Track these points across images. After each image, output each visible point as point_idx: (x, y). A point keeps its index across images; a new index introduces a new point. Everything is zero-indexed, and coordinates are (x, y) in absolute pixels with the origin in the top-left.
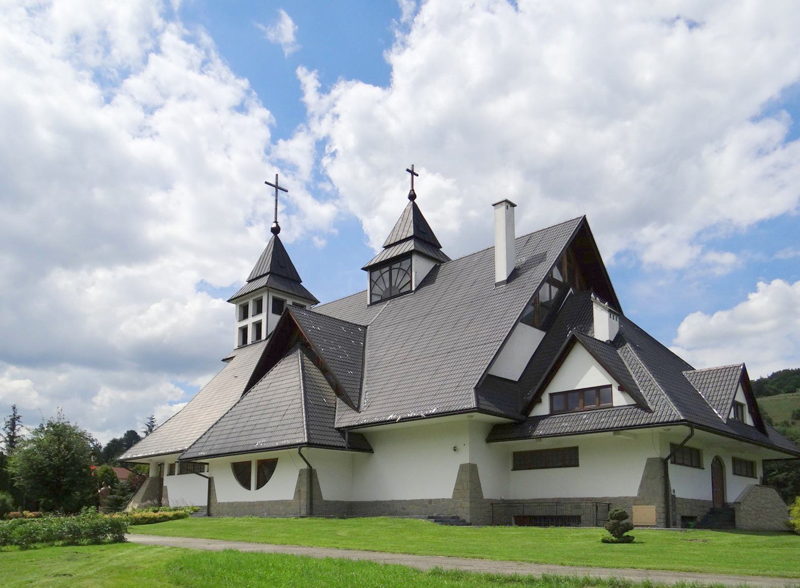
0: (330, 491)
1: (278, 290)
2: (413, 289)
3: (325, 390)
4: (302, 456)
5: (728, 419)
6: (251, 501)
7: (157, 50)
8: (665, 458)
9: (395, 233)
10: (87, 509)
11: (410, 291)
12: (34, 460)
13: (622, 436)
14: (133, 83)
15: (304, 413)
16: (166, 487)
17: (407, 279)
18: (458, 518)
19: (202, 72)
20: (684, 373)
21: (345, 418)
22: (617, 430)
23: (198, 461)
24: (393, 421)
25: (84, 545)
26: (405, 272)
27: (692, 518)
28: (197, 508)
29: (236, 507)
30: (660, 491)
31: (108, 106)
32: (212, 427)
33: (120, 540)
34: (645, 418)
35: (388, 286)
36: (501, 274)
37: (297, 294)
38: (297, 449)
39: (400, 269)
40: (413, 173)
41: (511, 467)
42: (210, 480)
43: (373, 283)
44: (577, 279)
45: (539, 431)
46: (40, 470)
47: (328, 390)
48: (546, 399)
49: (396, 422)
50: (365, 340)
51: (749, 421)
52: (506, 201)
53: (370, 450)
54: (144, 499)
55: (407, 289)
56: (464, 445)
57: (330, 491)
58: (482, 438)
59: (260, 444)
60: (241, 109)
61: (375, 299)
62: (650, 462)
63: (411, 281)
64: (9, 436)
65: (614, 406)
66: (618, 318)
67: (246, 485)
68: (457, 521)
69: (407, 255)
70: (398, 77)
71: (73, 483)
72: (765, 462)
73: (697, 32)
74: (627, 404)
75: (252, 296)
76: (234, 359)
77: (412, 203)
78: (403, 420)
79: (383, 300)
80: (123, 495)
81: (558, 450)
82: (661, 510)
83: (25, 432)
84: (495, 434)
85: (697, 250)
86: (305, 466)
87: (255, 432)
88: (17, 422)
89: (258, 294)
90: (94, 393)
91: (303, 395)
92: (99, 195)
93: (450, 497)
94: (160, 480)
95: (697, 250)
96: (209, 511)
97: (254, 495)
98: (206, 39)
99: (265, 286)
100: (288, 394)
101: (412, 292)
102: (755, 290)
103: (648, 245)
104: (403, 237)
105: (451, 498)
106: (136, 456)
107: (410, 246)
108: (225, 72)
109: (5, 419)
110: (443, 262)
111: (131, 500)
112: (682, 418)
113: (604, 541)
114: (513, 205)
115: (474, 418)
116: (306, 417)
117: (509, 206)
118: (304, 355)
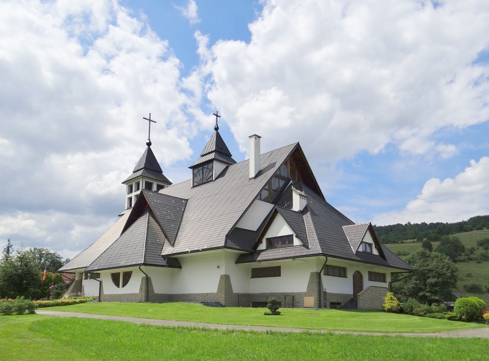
0: (158, 288)
1: (148, 177)
2: (214, 179)
3: (159, 235)
4: (141, 270)
5: (357, 252)
7: (114, 23)
8: (319, 272)
9: (207, 148)
10: (19, 297)
11: (212, 181)
12: (7, 271)
13: (297, 261)
14: (99, 42)
15: (144, 248)
16: (83, 286)
18: (219, 303)
19: (141, 36)
20: (343, 227)
21: (168, 250)
22: (294, 258)
23: (95, 272)
24: (187, 252)
25: (14, 315)
27: (339, 304)
28: (95, 297)
29: (113, 297)
30: (316, 288)
31: (84, 57)
32: (102, 254)
33: (33, 313)
34: (305, 252)
35: (201, 177)
36: (252, 174)
37: (159, 179)
38: (138, 267)
39: (207, 168)
40: (217, 116)
41: (250, 276)
42: (101, 282)
44: (296, 175)
45: (259, 258)
46: (10, 277)
47: (162, 235)
48: (264, 241)
50: (185, 207)
51: (375, 252)
52: (255, 135)
53: (180, 267)
54: (73, 292)
57: (158, 288)
58: (233, 262)
59: (122, 263)
60: (164, 58)
61: (195, 184)
62: (312, 274)
63: (213, 175)
64: (6, 256)
65: (294, 245)
66: (306, 199)
67: (117, 285)
68: (217, 304)
69: (211, 161)
70: (254, 38)
71: (28, 284)
72: (392, 274)
73: (440, 10)
74: (299, 245)
75: (134, 181)
76: (124, 215)
77: (216, 132)
78: (192, 252)
79: (199, 185)
80: (62, 290)
81: (272, 268)
82: (316, 299)
83: (14, 255)
84: (240, 259)
85: (433, 143)
86: (145, 276)
87: (121, 257)
88: (10, 249)
90: (72, 228)
91: (145, 238)
92: (79, 111)
93: (216, 292)
94: (81, 281)
95: (433, 143)
96: (100, 299)
97: (121, 291)
98: (144, 16)
99: (141, 175)
100: (139, 237)
102: (469, 165)
103: (403, 140)
104: (210, 151)
105: (216, 292)
106: (67, 269)
107: (212, 156)
108: (154, 35)
109: (3, 247)
110: (231, 164)
111: (65, 293)
112: (321, 252)
113: (266, 314)
114: (259, 137)
115: (226, 251)
116: (145, 250)
117: (257, 137)
118: (150, 216)
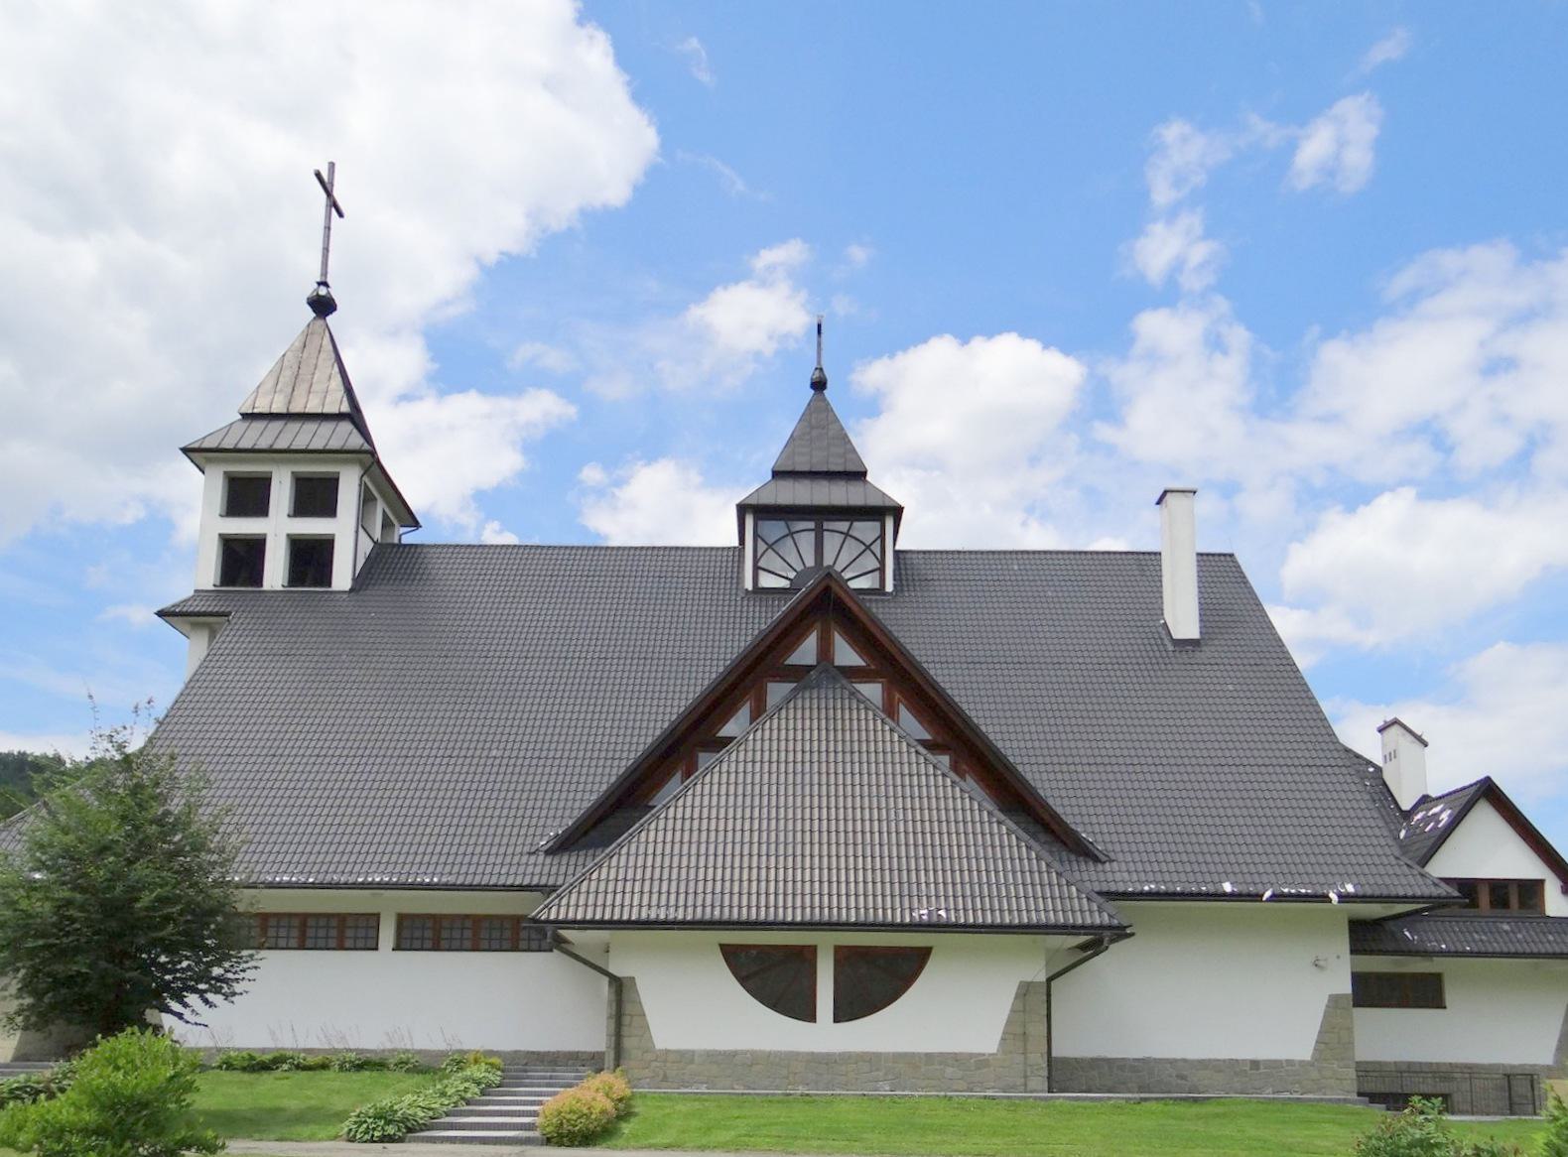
2: (889, 587)
6: (815, 1051)
26: (863, 547)
49: (1261, 901)
56: (1338, 957)
89: (263, 462)
101: (885, 594)
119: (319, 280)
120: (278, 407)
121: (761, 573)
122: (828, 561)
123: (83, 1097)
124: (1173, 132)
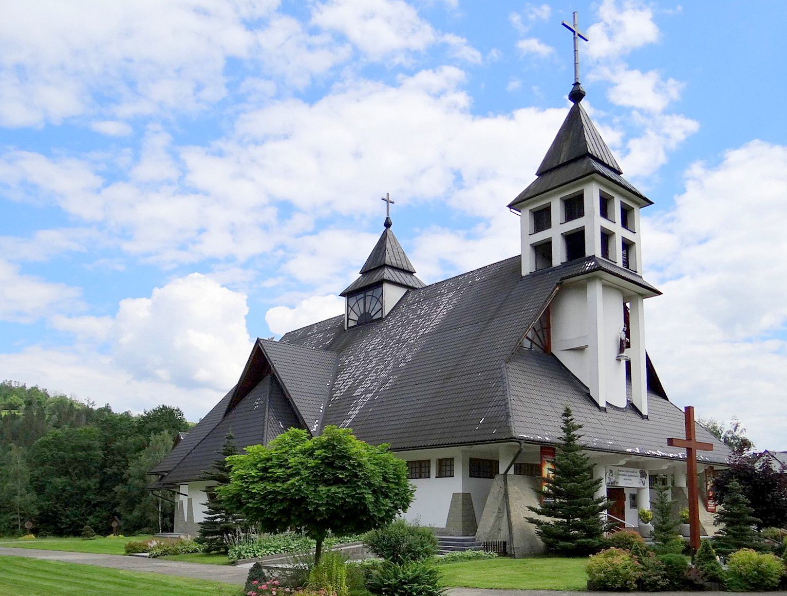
17: (378, 307)
43: (350, 309)
55: (378, 316)
119: (574, 83)
120: (555, 165)
121: (349, 320)
122: (367, 311)
123: (32, 497)
124: (546, 8)
